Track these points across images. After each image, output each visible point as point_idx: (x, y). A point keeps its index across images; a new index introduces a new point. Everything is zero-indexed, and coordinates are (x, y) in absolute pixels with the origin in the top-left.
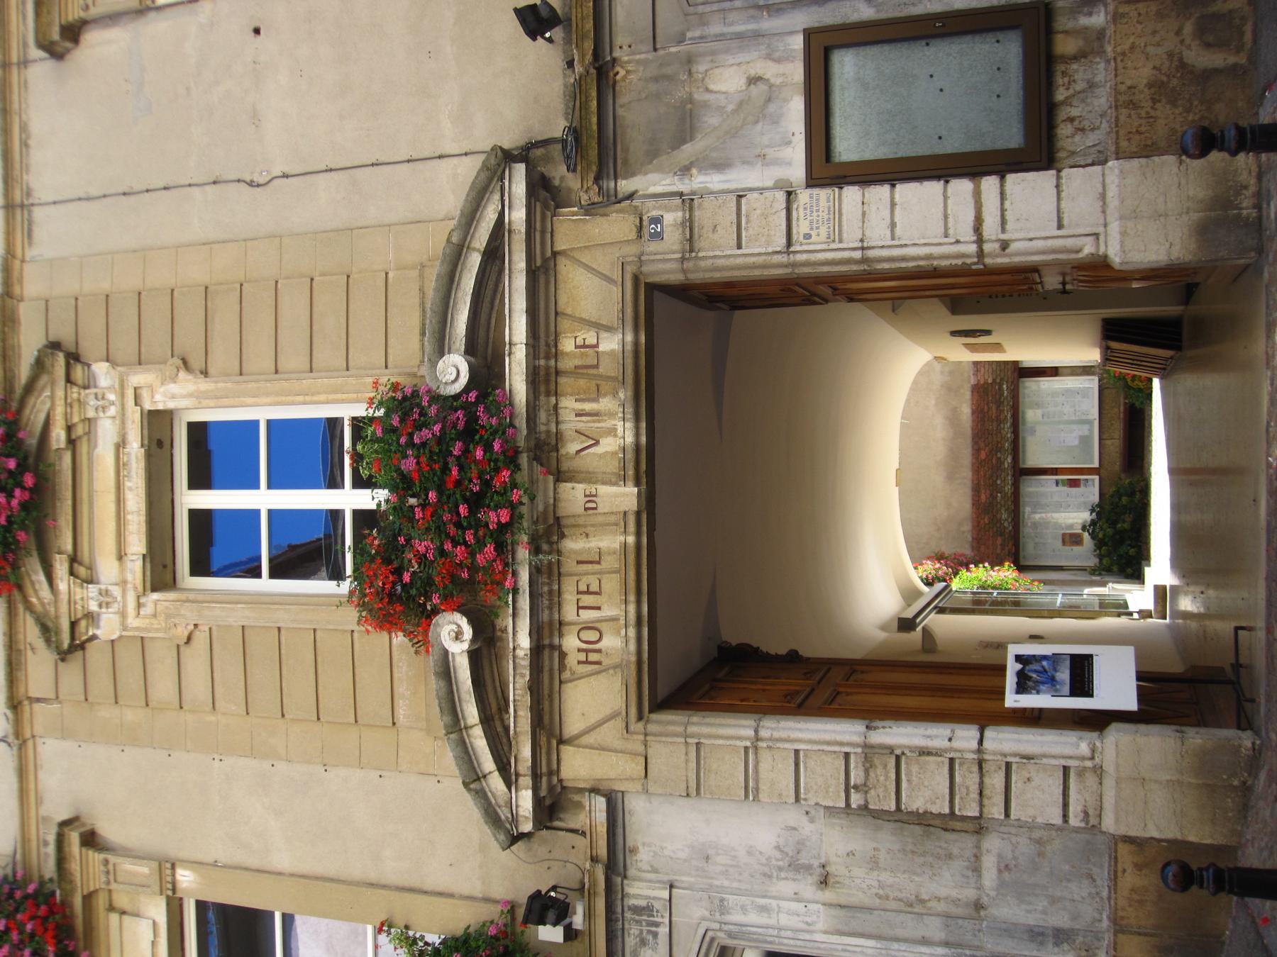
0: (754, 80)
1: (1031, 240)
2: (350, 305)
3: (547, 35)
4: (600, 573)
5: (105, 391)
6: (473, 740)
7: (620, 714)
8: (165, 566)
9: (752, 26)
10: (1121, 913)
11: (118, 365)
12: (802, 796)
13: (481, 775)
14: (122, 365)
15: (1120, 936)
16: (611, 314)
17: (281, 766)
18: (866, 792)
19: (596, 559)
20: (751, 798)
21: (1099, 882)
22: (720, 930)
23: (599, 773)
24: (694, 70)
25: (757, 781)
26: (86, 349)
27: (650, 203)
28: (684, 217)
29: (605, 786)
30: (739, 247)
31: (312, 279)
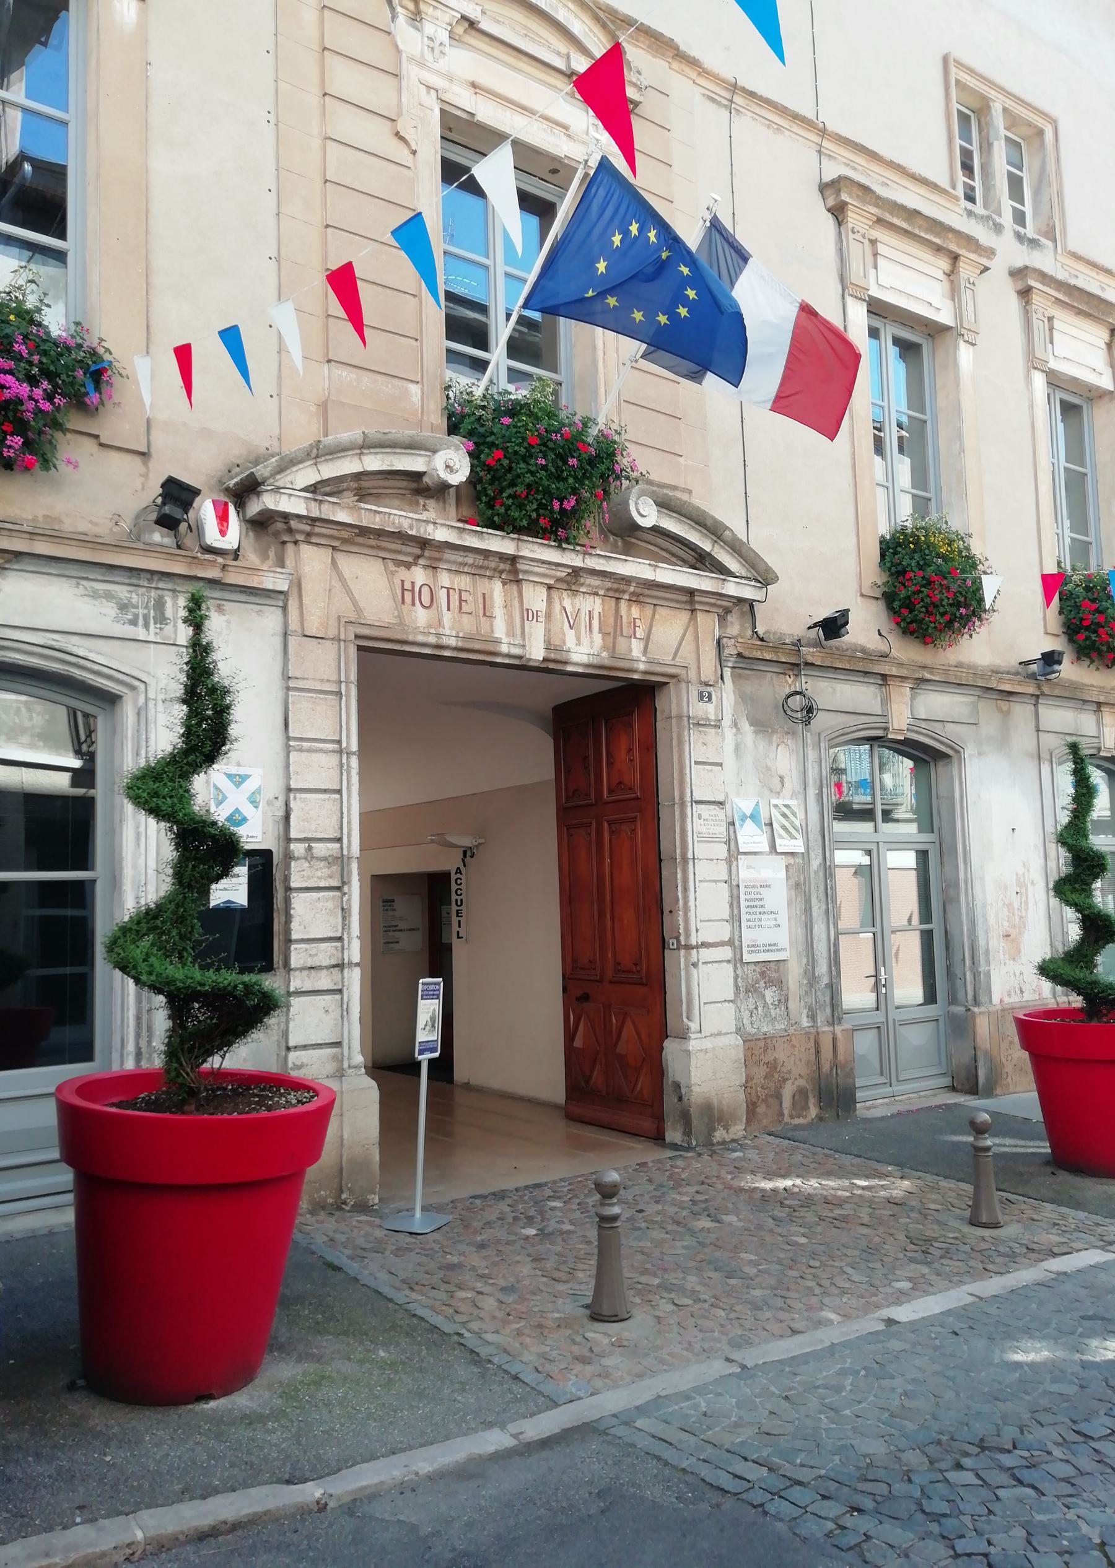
2: (663, 416)
6: (349, 458)
12: (298, 795)
18: (306, 858)
19: (487, 612)
22: (146, 698)
25: (309, 751)
30: (697, 763)
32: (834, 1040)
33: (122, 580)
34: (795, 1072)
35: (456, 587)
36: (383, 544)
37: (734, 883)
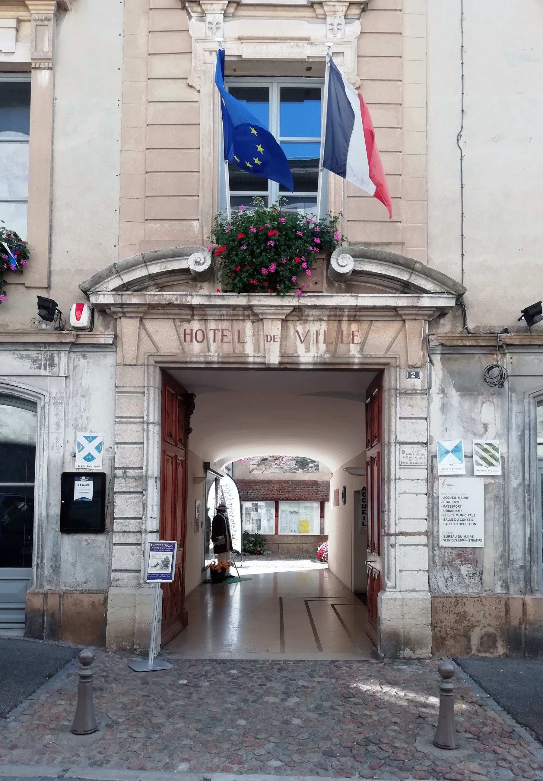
0: (486, 427)
1: (395, 558)
3: (523, 318)
4: (233, 343)
5: (343, 31)
6: (140, 269)
7: (158, 352)
8: (235, 70)
9: (514, 426)
10: (69, 596)
11: (358, 40)
12: (119, 446)
13: (120, 274)
14: (358, 44)
15: (59, 596)
16: (369, 350)
17: (118, 146)
18: (123, 477)
19: (240, 340)
20: (117, 420)
21: (84, 585)
22: (45, 403)
23: (125, 339)
24: (494, 396)
25: (126, 423)
26: (370, 16)
27: (427, 373)
28: (418, 390)
29: (118, 342)
30: (400, 418)
31: (400, 175)
32: (524, 604)
33: (32, 348)
34: (484, 622)
35: (220, 328)
36: (168, 311)
37: (435, 495)
